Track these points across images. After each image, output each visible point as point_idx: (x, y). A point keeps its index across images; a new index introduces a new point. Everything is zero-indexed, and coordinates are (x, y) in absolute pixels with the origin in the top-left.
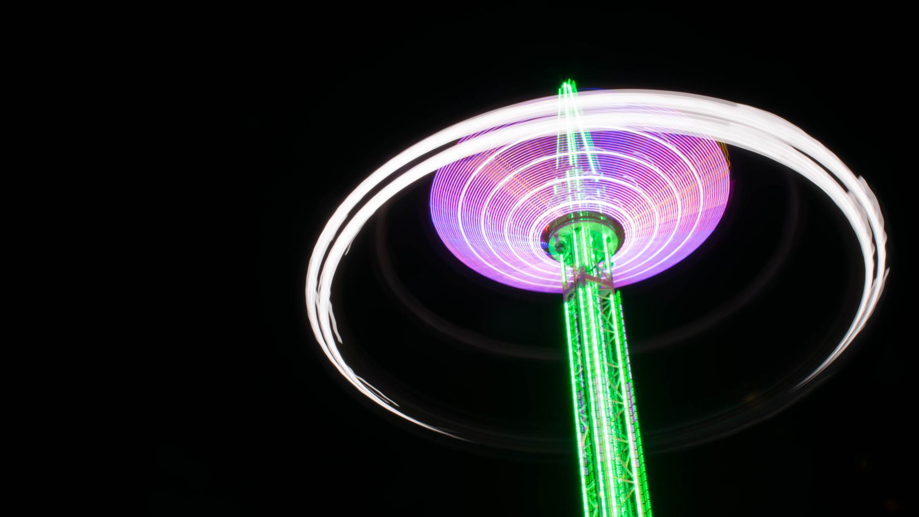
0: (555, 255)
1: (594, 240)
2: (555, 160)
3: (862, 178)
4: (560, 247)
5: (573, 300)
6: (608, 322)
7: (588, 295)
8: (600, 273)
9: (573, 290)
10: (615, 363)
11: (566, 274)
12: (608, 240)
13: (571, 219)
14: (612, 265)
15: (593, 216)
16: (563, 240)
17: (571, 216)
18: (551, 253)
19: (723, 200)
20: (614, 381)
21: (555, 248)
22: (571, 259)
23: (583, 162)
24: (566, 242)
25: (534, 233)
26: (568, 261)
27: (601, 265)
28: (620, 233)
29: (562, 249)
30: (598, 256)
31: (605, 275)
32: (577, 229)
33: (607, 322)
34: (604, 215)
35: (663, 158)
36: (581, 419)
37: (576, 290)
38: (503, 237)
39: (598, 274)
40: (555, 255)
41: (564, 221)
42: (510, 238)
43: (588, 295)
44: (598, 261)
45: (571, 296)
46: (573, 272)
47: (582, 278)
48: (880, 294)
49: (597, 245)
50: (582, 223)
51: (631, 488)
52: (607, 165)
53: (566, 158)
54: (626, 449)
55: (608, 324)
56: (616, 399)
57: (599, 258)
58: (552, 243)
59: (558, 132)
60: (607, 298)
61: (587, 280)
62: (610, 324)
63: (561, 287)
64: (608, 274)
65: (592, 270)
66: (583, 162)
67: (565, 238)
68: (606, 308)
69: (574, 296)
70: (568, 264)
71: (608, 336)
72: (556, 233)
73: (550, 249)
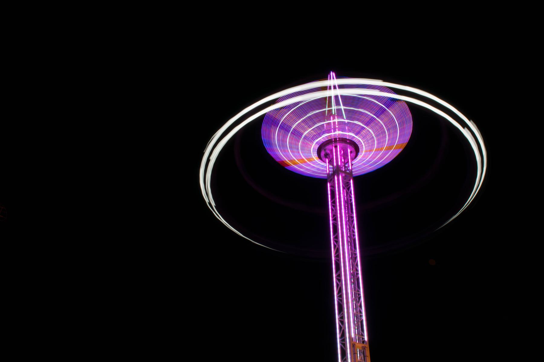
0: (324, 158)
1: (344, 152)
2: (326, 111)
3: (471, 121)
4: (326, 156)
5: (332, 181)
6: (355, 265)
7: (339, 181)
8: (346, 169)
9: (332, 177)
10: (352, 214)
11: (329, 169)
12: (351, 152)
13: (332, 142)
14: (352, 165)
15: (343, 140)
16: (328, 152)
17: (332, 140)
18: (322, 158)
19: (407, 138)
20: (351, 223)
21: (324, 156)
22: (331, 162)
23: (339, 111)
24: (330, 153)
25: (314, 146)
26: (330, 163)
27: (347, 165)
28: (356, 149)
29: (328, 156)
30: (345, 160)
31: (349, 170)
32: (336, 147)
33: (348, 194)
34: (349, 140)
35: (378, 113)
36: (332, 206)
37: (334, 177)
38: (299, 152)
39: (345, 170)
40: (324, 158)
41: (329, 142)
42: (302, 153)
43: (339, 181)
44: (345, 163)
45: (331, 180)
46: (333, 168)
47: (337, 171)
48: (483, 140)
49: (345, 155)
50: (338, 144)
51: (361, 318)
52: (351, 115)
53: (331, 110)
54: (352, 220)
55: (349, 195)
56: (352, 232)
57: (346, 162)
58: (323, 153)
59: (328, 86)
60: (349, 182)
61: (339, 172)
62: (356, 267)
63: (326, 176)
64: (350, 170)
65: (342, 167)
66: (339, 111)
67: (329, 151)
68: (348, 187)
69: (333, 180)
70: (330, 164)
71: (349, 200)
72: (325, 148)
73: (321, 156)
